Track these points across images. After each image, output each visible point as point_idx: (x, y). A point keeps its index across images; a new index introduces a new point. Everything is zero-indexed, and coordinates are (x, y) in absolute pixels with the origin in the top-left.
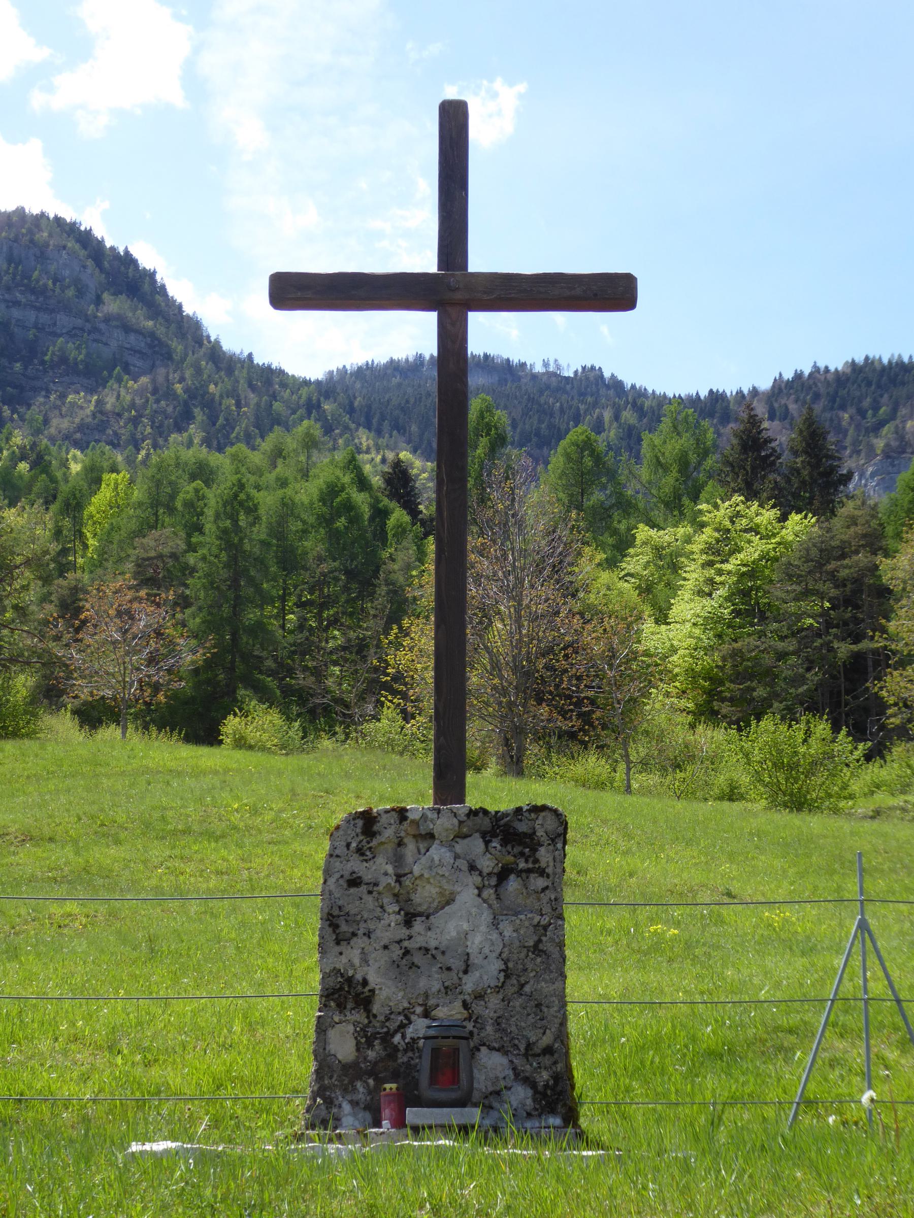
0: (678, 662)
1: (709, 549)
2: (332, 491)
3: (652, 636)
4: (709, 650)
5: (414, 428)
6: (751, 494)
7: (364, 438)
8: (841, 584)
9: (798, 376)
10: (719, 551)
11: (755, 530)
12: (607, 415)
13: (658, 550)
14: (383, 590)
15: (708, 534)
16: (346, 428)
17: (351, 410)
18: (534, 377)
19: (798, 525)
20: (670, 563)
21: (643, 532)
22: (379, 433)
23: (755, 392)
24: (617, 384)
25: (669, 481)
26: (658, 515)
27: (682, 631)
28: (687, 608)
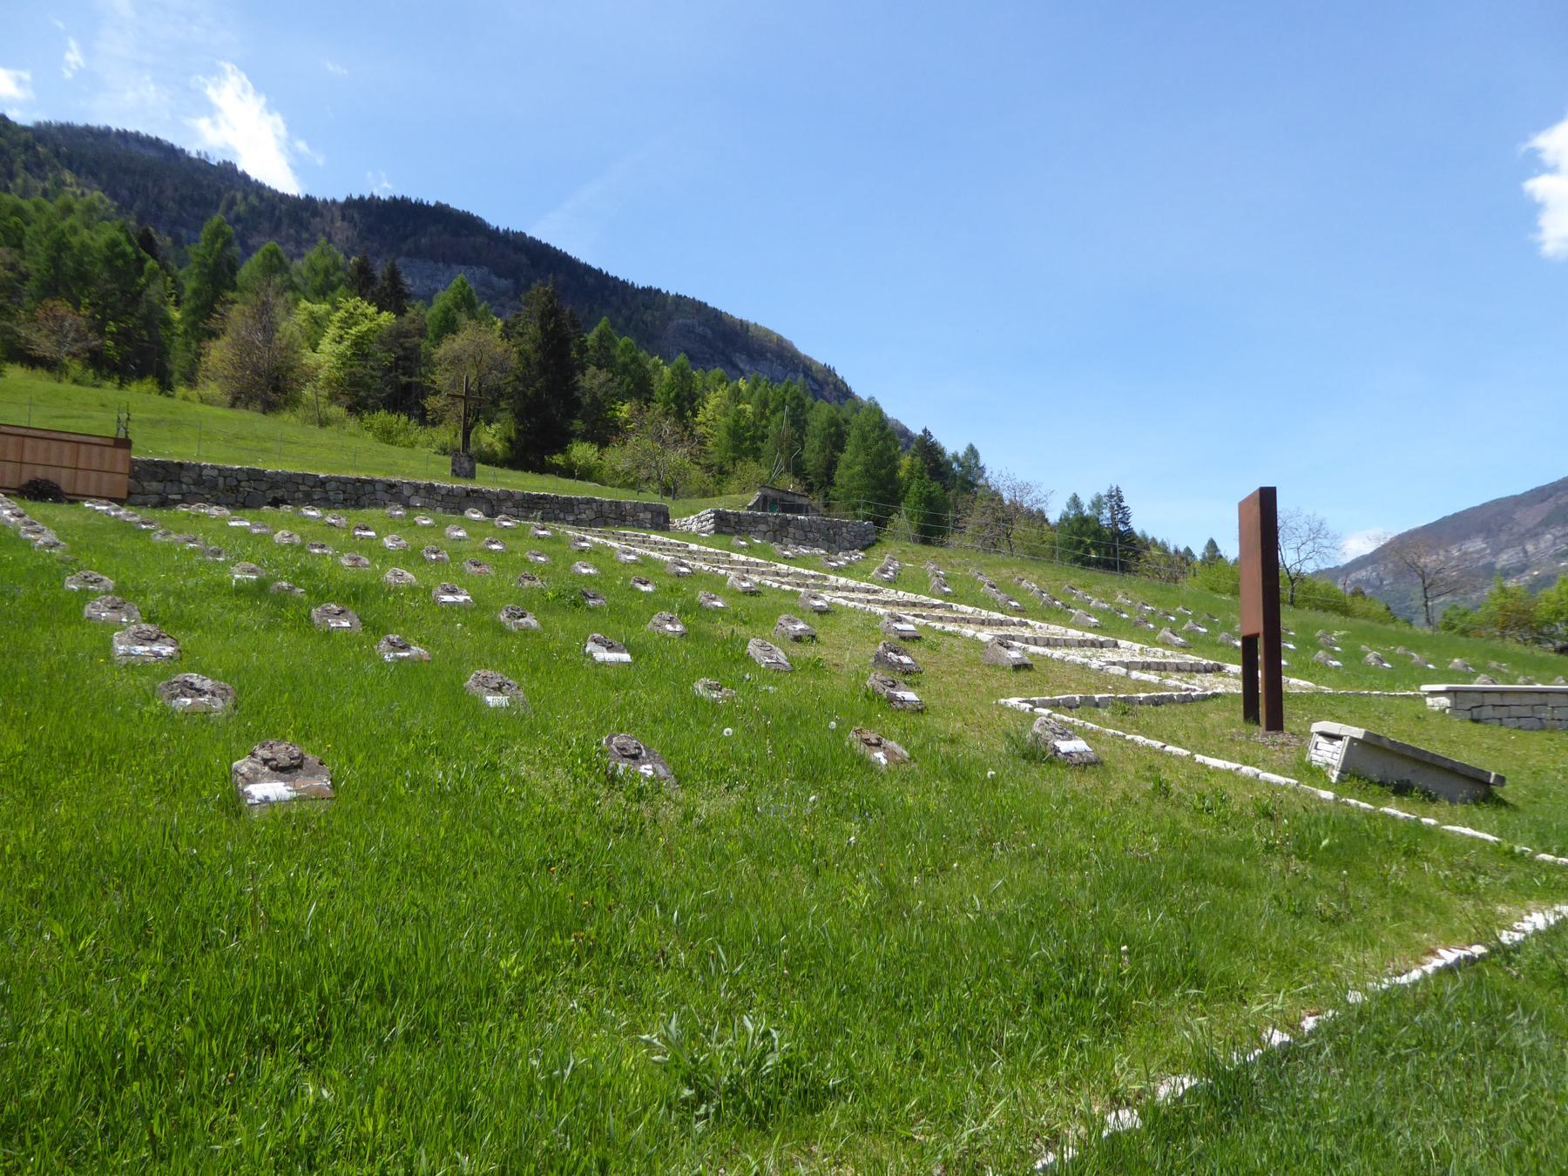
0: (322, 374)
1: (342, 320)
2: (113, 244)
3: (309, 358)
4: (339, 369)
5: (104, 176)
6: (363, 297)
7: (68, 177)
8: (405, 349)
9: (361, 198)
10: (348, 322)
11: (365, 316)
12: (239, 196)
13: (311, 313)
14: (144, 305)
15: (341, 314)
16: (54, 167)
17: (57, 154)
18: (190, 159)
19: (386, 318)
20: (318, 323)
21: (304, 304)
22: (78, 173)
23: (334, 202)
24: (245, 177)
25: (319, 280)
26: (311, 297)
27: (326, 356)
28: (326, 345)
